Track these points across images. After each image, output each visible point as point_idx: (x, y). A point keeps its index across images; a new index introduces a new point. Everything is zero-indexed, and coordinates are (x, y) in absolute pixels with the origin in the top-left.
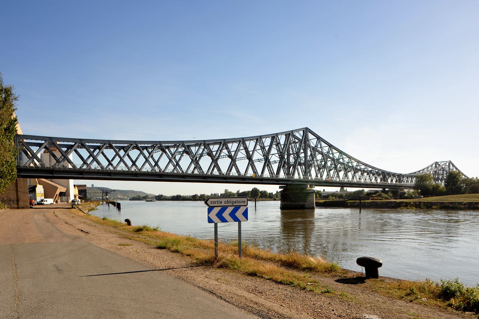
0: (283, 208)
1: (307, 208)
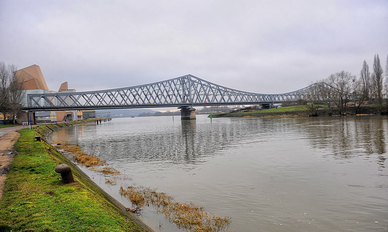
0: (182, 119)
1: (191, 119)
